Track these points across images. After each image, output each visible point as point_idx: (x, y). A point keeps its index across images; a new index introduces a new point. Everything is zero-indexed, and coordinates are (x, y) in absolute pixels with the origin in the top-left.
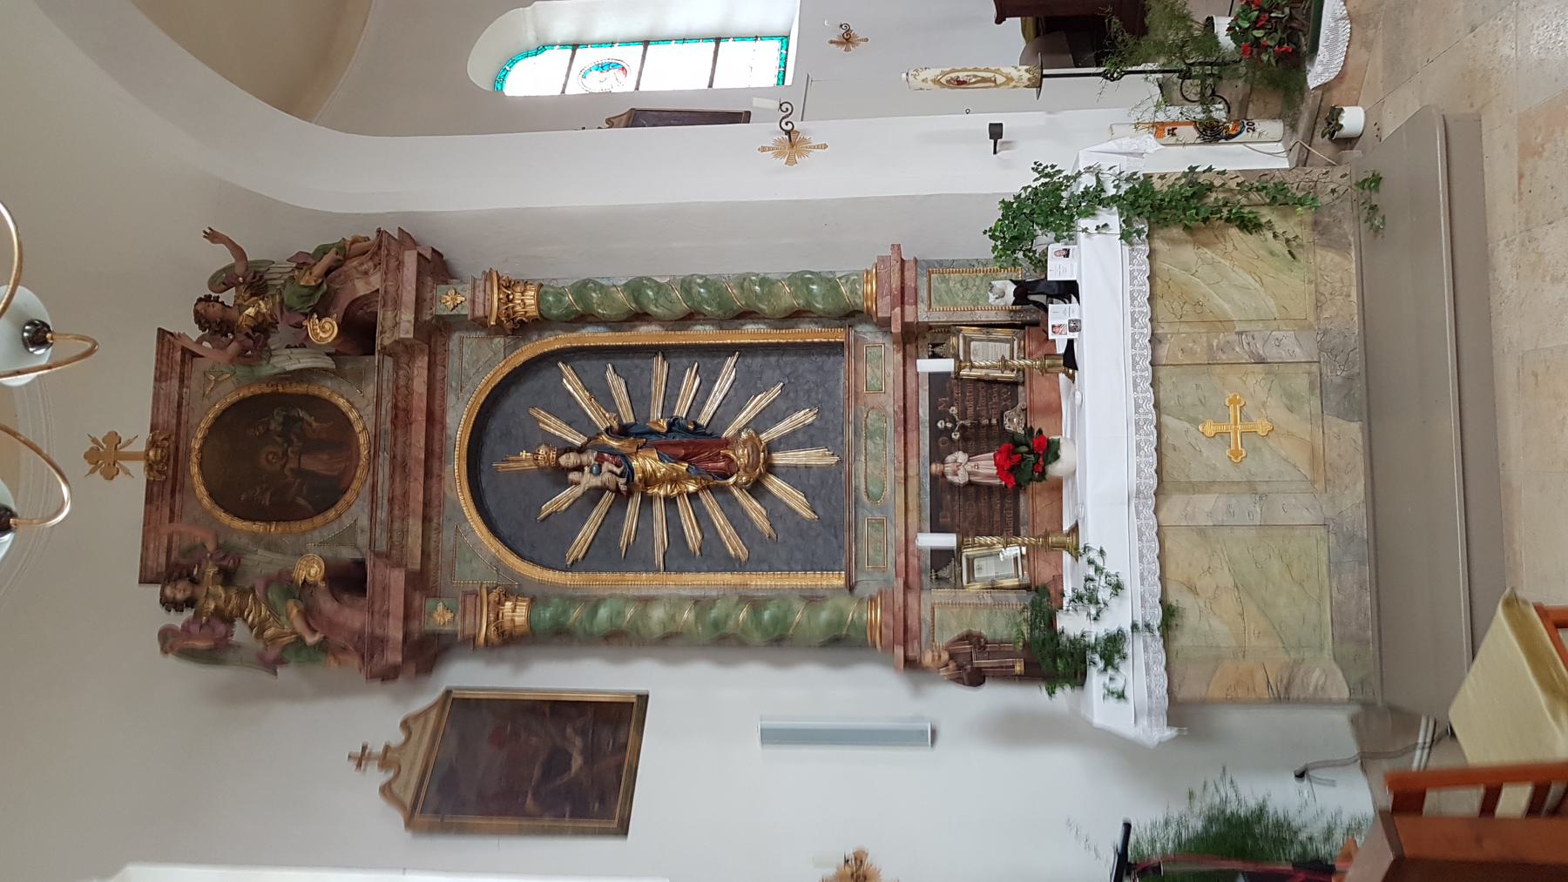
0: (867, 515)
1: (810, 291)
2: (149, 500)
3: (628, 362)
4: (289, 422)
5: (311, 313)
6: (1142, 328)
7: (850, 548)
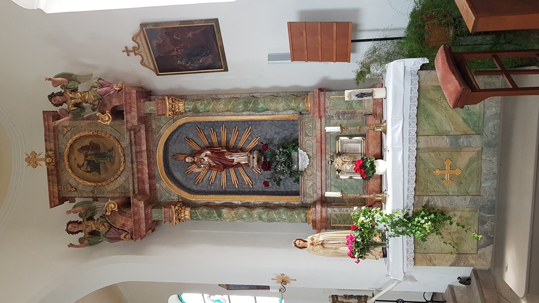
6: (411, 192)
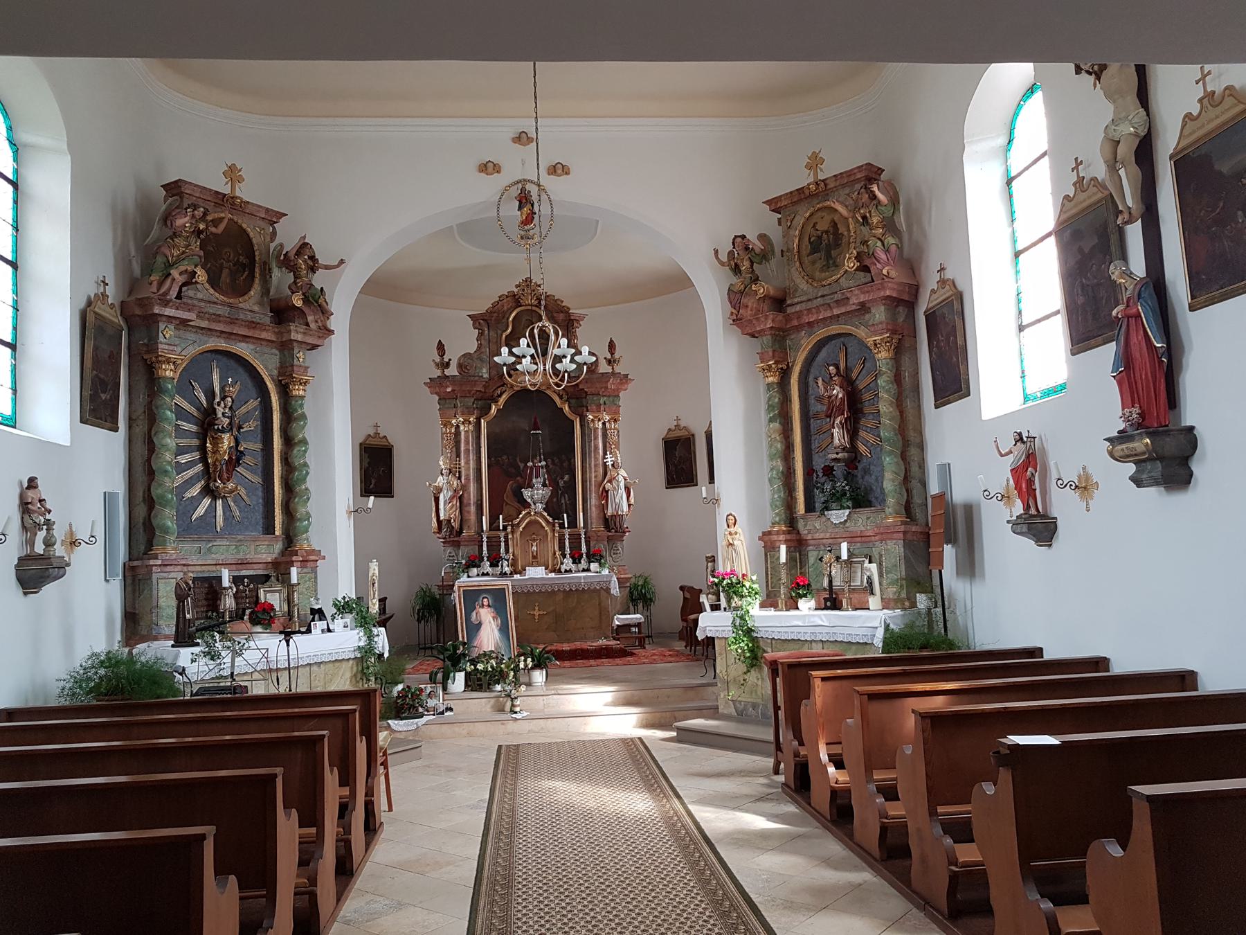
0: (204, 546)
1: (305, 521)
2: (217, 192)
3: (259, 432)
4: (244, 266)
5: (305, 296)
7: (190, 538)
